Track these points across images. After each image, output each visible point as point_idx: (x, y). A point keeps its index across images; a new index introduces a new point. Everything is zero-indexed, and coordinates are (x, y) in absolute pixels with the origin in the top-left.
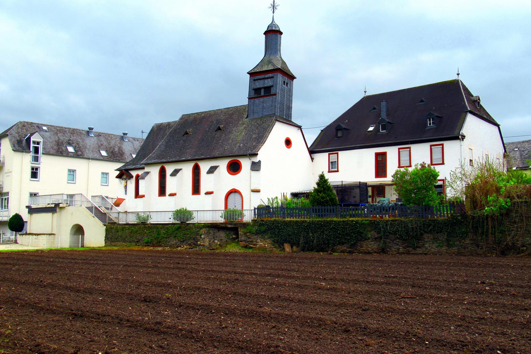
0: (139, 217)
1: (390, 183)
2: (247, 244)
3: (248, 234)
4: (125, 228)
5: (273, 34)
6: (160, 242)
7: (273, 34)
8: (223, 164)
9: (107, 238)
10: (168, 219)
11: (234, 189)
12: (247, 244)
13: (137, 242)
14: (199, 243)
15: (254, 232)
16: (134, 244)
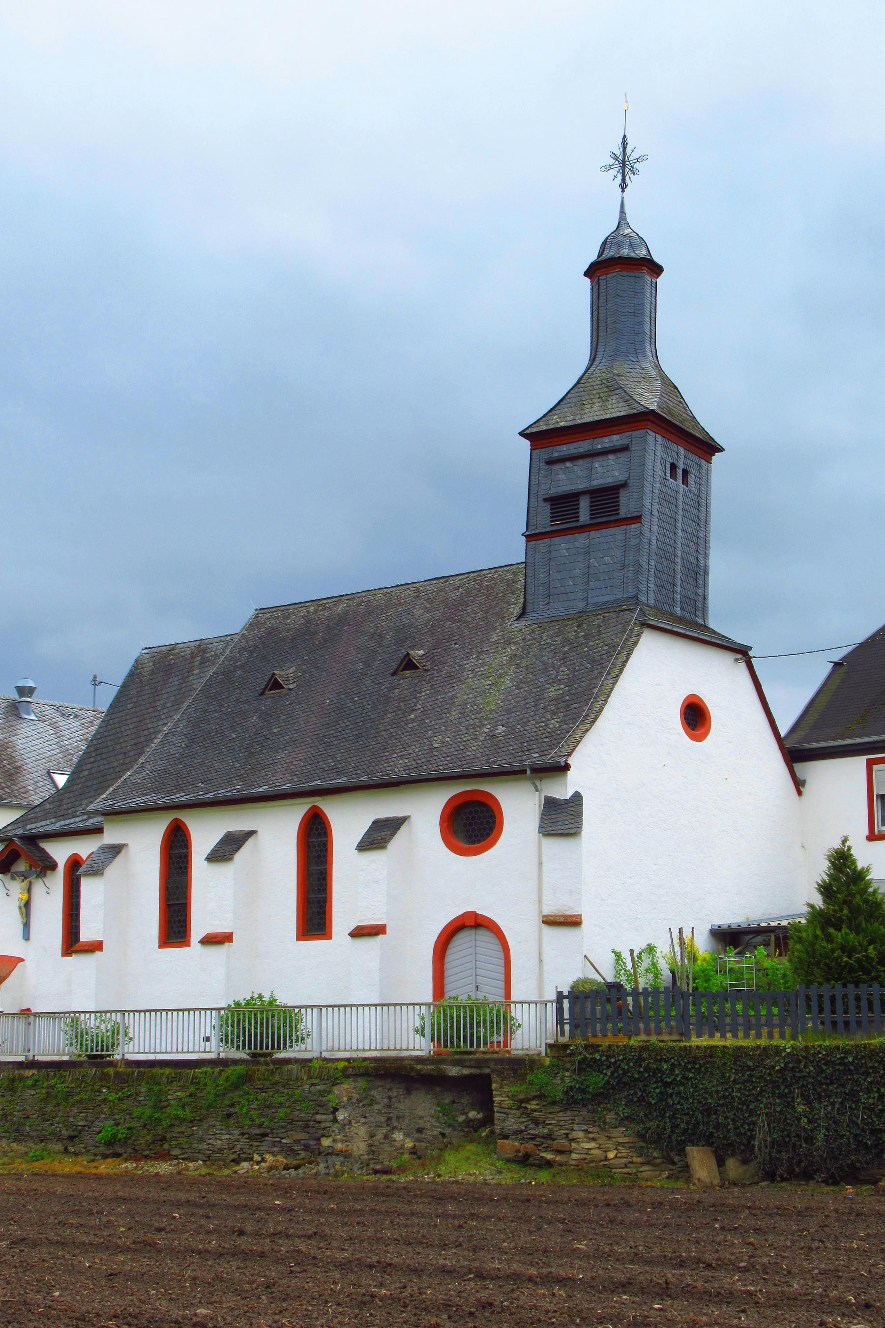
0: (78, 1034)
1: (588, 523)
2: (530, 1146)
3: (533, 1105)
4: (22, 1079)
5: (622, 274)
6: (164, 1139)
7: (622, 274)
8: (425, 812)
10: (195, 1040)
11: (474, 914)
12: (530, 1146)
13: (71, 1138)
15: (559, 1096)
16: (59, 1147)
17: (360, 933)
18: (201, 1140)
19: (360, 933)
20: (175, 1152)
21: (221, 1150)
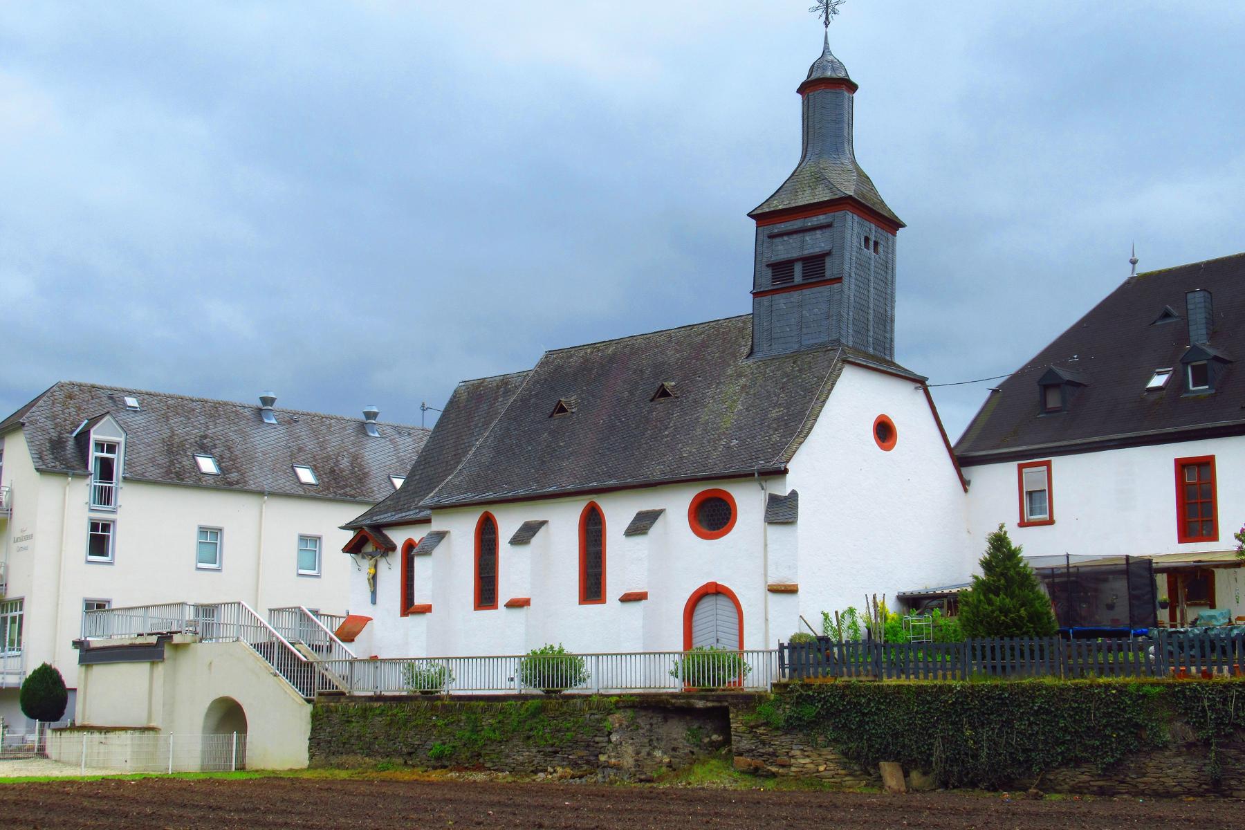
0: (414, 676)
2: (759, 761)
3: (761, 730)
4: (371, 709)
5: (826, 90)
6: (479, 755)
7: (826, 90)
9: (316, 743)
10: (502, 680)
12: (759, 761)
13: (410, 754)
14: (602, 758)
16: (400, 761)
17: (628, 598)
18: (508, 756)
19: (628, 598)
20: (488, 765)
21: (522, 764)
